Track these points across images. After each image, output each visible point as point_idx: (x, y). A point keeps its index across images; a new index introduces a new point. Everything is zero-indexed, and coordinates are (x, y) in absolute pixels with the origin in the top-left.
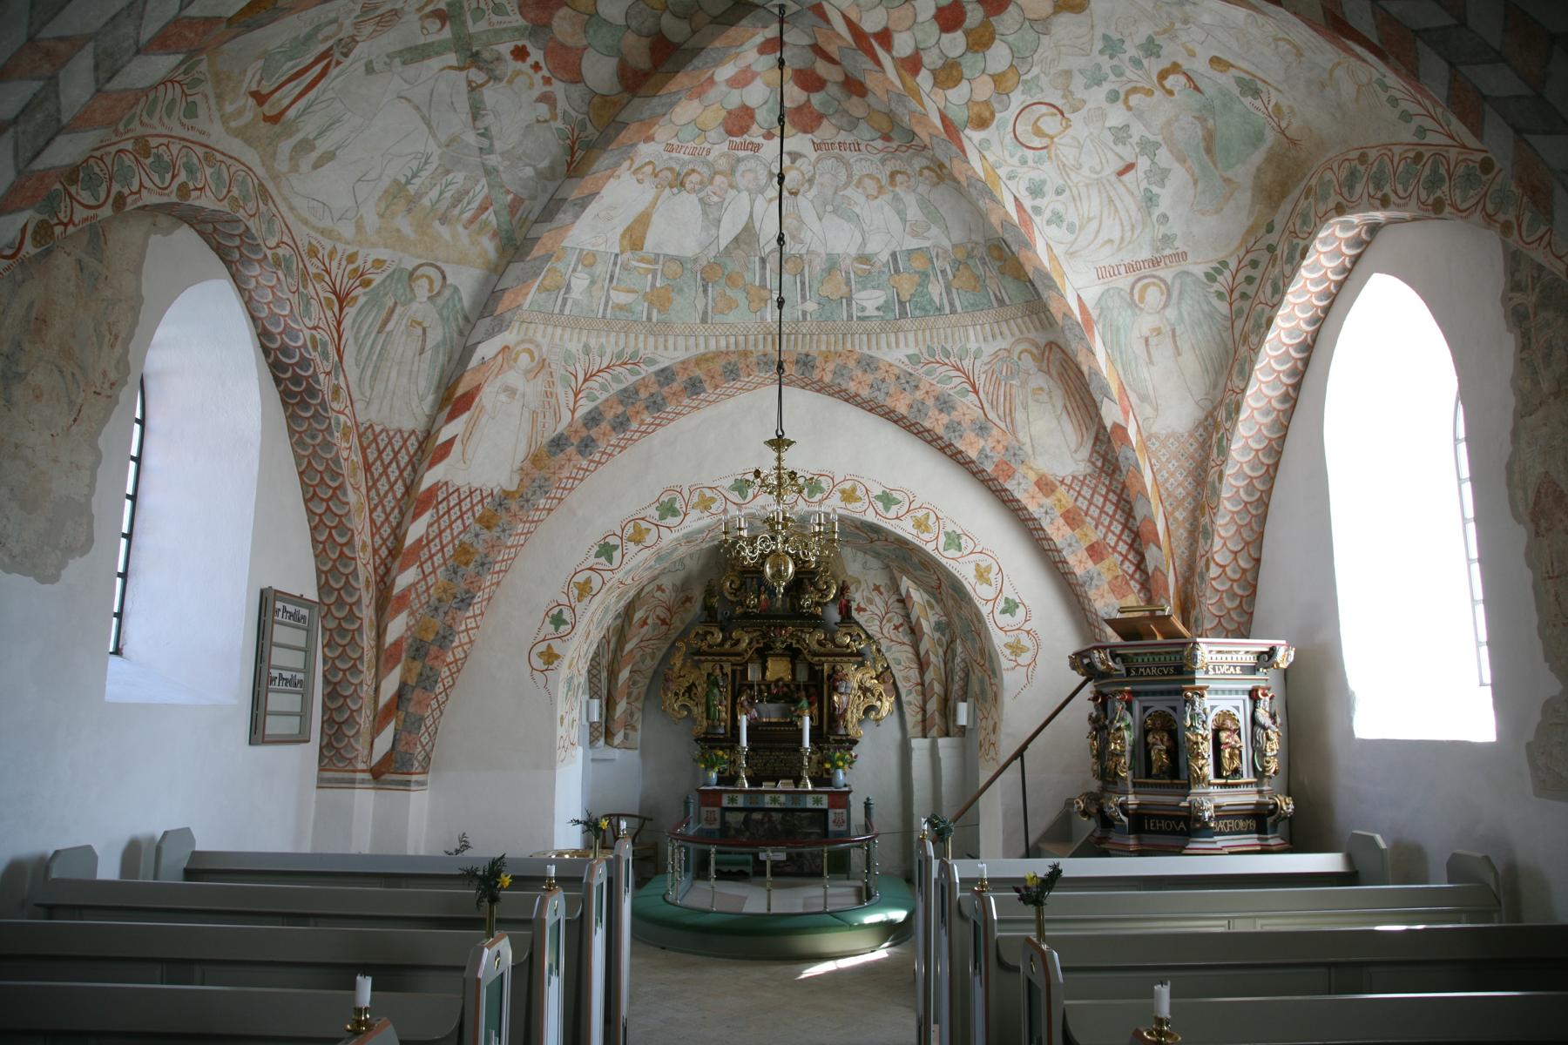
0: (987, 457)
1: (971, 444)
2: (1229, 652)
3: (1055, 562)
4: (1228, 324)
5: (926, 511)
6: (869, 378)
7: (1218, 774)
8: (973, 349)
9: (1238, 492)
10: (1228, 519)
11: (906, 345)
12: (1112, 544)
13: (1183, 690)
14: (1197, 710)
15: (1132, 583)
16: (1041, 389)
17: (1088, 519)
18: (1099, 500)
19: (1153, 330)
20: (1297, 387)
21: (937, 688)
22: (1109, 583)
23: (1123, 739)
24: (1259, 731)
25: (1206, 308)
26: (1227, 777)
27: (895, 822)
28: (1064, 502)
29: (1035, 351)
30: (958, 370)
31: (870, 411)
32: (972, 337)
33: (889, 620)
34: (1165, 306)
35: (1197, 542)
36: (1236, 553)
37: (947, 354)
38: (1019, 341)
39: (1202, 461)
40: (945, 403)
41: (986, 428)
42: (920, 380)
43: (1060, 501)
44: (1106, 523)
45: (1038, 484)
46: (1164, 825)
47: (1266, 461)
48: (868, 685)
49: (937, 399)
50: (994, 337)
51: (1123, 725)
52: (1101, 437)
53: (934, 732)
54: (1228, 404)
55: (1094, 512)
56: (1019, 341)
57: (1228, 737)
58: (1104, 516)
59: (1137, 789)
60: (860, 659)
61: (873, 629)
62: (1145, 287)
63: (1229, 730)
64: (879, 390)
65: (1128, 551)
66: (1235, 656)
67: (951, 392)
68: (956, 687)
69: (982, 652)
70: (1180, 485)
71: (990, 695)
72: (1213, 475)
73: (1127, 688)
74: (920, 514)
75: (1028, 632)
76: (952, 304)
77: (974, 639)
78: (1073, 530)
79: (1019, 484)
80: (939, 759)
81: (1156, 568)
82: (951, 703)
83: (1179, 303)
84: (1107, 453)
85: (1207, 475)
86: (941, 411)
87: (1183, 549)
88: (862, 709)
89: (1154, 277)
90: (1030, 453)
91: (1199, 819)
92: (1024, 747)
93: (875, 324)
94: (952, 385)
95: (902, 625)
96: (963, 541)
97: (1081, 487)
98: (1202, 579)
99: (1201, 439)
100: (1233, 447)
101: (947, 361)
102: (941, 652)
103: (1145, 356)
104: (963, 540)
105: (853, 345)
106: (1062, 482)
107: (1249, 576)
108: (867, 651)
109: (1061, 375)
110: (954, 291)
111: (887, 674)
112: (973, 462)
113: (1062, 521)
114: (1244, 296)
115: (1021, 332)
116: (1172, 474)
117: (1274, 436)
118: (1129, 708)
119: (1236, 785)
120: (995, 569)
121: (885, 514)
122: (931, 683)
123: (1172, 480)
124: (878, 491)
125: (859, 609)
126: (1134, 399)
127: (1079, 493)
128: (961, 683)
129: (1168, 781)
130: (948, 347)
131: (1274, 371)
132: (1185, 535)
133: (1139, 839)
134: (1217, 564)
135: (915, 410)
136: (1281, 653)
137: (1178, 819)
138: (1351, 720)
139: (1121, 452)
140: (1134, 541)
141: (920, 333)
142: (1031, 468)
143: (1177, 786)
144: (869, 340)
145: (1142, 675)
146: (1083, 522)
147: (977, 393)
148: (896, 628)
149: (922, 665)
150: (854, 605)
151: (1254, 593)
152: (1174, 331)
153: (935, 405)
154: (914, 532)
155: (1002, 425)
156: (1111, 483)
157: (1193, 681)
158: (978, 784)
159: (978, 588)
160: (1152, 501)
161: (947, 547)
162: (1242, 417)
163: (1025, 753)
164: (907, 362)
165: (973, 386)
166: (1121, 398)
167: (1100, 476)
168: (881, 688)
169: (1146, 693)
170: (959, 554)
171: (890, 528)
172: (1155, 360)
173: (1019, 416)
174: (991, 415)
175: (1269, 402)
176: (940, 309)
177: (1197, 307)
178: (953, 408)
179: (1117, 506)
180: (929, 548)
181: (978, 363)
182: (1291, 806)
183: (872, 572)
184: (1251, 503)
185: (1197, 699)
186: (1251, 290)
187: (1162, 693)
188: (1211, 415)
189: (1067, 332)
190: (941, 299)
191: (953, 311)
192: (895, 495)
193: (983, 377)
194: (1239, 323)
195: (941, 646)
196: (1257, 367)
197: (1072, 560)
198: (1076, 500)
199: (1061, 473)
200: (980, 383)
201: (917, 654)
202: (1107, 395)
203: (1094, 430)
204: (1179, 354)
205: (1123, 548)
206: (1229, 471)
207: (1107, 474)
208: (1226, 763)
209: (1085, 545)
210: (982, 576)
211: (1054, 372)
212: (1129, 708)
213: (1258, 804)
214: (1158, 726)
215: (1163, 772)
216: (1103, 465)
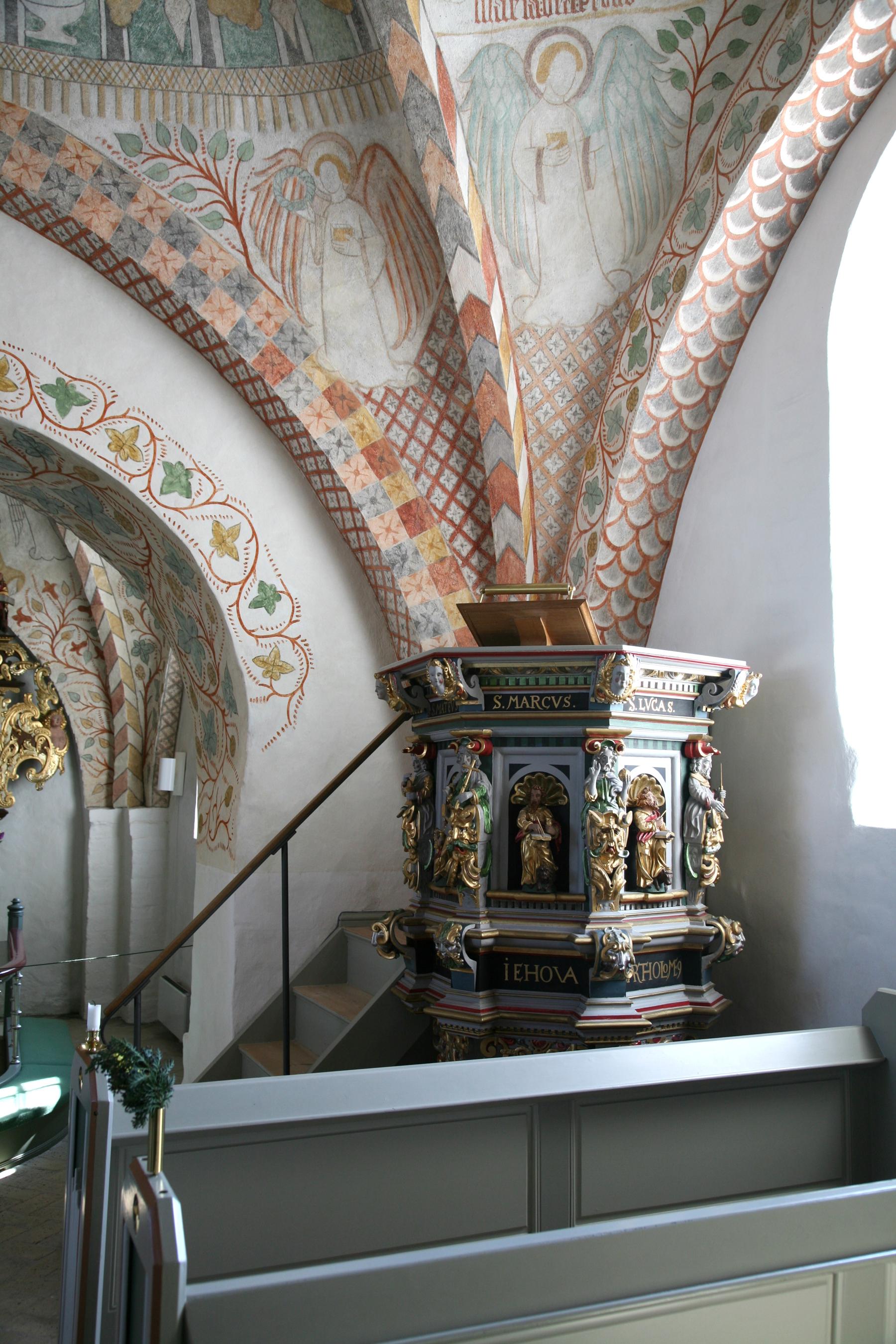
0: (247, 337)
1: (222, 311)
2: (660, 675)
3: (345, 531)
4: (682, 134)
5: (132, 423)
6: (44, 161)
7: (631, 886)
8: (238, 144)
9: (656, 427)
10: (635, 471)
11: (118, 114)
12: (440, 507)
13: (587, 736)
14: (609, 774)
15: (466, 571)
16: (349, 231)
17: (405, 462)
18: (425, 432)
19: (553, 137)
20: (778, 253)
21: (132, 737)
22: (431, 568)
23: (474, 820)
24: (696, 812)
25: (649, 101)
26: (646, 890)
27: (60, 928)
28: (368, 429)
29: (346, 161)
30: (209, 177)
31: (43, 232)
32: (238, 119)
33: (66, 637)
34: (580, 93)
35: (574, 510)
36: (638, 529)
37: (191, 144)
38: (319, 138)
39: (600, 379)
40: (181, 232)
41: (249, 289)
42: (139, 185)
43: (362, 427)
44: (433, 472)
45: (328, 394)
46: (538, 973)
47: (706, 380)
48: (27, 729)
49: (167, 223)
50: (277, 124)
51: (477, 795)
52: (439, 325)
53: (124, 799)
54: (661, 278)
55: (416, 451)
56: (319, 138)
57: (650, 821)
58: (430, 458)
59: (494, 910)
60: (17, 690)
61: (41, 648)
62: (553, 50)
63: (651, 808)
64: (62, 187)
65: (464, 519)
66: (668, 681)
67: (193, 217)
68: (160, 737)
69: (214, 672)
70: (560, 415)
71: (223, 742)
72: (617, 400)
73: (486, 731)
74: (123, 427)
75: (294, 641)
76: (207, 47)
77: (200, 651)
78: (380, 477)
79: (298, 390)
80: (130, 839)
81: (509, 548)
82: (151, 760)
83: (604, 89)
84: (446, 352)
85: (604, 402)
86: (173, 245)
87: (551, 520)
88: (16, 764)
89: (569, 31)
90: (320, 341)
91: (607, 966)
92: (290, 831)
93: (61, 60)
94: (195, 204)
95: (84, 644)
96: (194, 482)
97: (399, 408)
98: (580, 567)
99: (603, 340)
100: (664, 348)
101: (189, 157)
102: (140, 685)
103: (532, 184)
104: (195, 480)
105: (15, 93)
106: (368, 397)
107: (652, 569)
108: (29, 679)
109: (385, 209)
110: (213, 19)
111: (57, 715)
112: (222, 344)
113: (363, 460)
114: (720, 80)
115: (325, 121)
116: (549, 396)
117: (726, 339)
118: (486, 766)
119: (657, 903)
120: (246, 533)
121: (58, 419)
122: (124, 728)
123: (547, 406)
124: (48, 376)
125: (20, 618)
126: (503, 260)
127: (394, 418)
128: (168, 730)
129: (551, 897)
130: (194, 130)
131: (754, 216)
132: (557, 498)
133: (493, 998)
134: (609, 544)
135: (126, 234)
136: (741, 679)
137: (564, 962)
138: (846, 796)
139: (474, 347)
140: (474, 503)
141: (144, 95)
142: (319, 367)
143: (565, 905)
144: (47, 91)
145: (513, 708)
146: (397, 466)
147: (238, 224)
148: (76, 648)
149: (112, 704)
150: (12, 611)
151: (656, 595)
152: (587, 141)
153: (162, 234)
154: (111, 456)
155: (277, 288)
156: (447, 406)
157: (605, 722)
158: (191, 907)
159: (216, 561)
160: (514, 436)
161: (167, 487)
162: (688, 295)
163: (290, 843)
164: (117, 146)
165: (233, 210)
166: (484, 254)
167: (430, 392)
168: (47, 734)
169: (518, 741)
170: (186, 502)
171: (66, 443)
172: (547, 194)
173: (307, 274)
174: (260, 268)
175: (733, 275)
176: (184, 54)
177: (633, 99)
178: (195, 245)
179: (453, 444)
180: (136, 487)
181: (245, 169)
182: (741, 938)
183: (44, 564)
184: (672, 449)
185: (609, 753)
186: (733, 68)
187: (546, 741)
188: (625, 299)
189: (411, 113)
190: (188, 34)
191: (209, 62)
192: (80, 388)
193: (251, 197)
194: (701, 134)
195: (141, 676)
196: (730, 204)
197: (375, 526)
198: (388, 429)
199: (367, 383)
200: (246, 205)
201: (105, 688)
202: (464, 243)
203: (429, 312)
204: (590, 186)
205: (456, 513)
206: (651, 389)
207: (443, 389)
208: (644, 863)
209: (397, 502)
210: (223, 542)
211: (373, 202)
212: (486, 766)
213: (690, 935)
214: (536, 798)
215: (541, 882)
216: (439, 373)
